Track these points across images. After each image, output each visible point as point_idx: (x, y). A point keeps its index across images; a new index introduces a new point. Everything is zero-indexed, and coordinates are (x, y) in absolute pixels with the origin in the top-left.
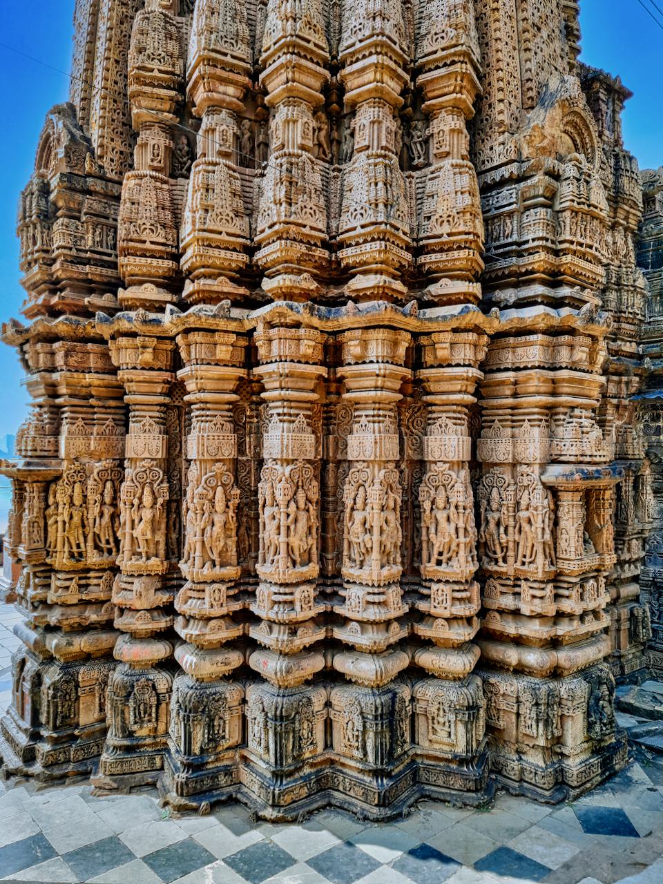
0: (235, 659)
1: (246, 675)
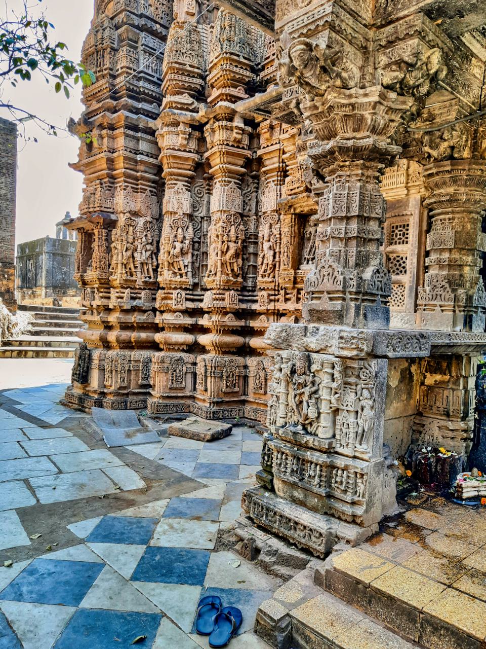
0: (188, 338)
1: (195, 348)
